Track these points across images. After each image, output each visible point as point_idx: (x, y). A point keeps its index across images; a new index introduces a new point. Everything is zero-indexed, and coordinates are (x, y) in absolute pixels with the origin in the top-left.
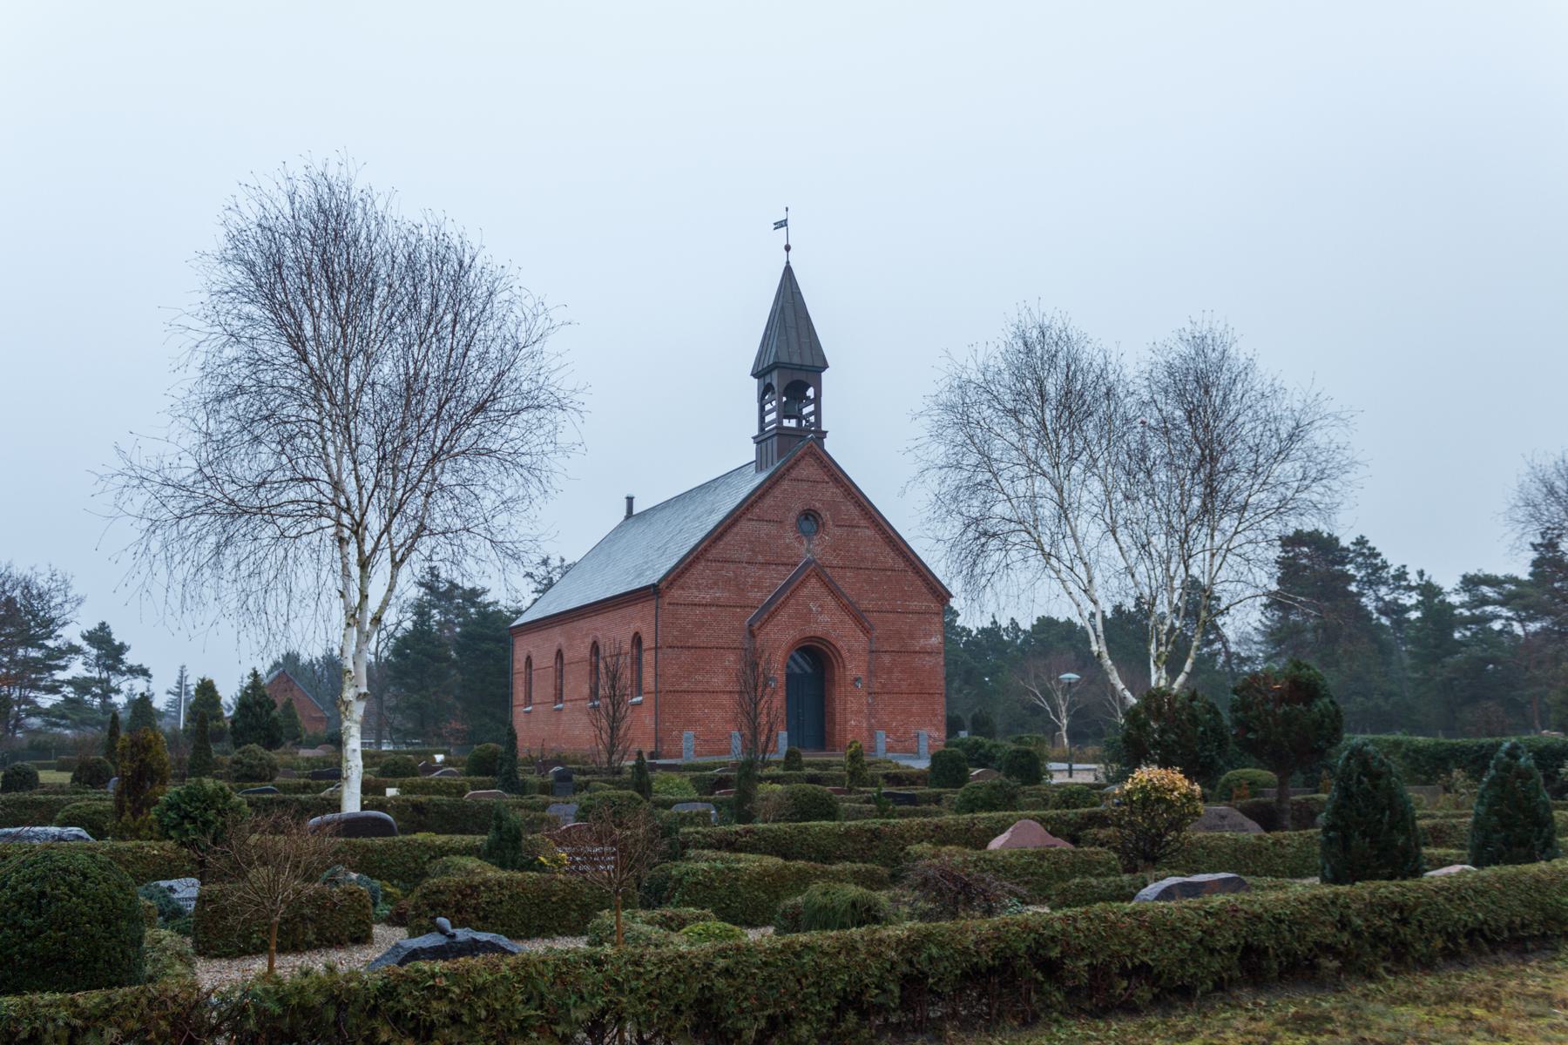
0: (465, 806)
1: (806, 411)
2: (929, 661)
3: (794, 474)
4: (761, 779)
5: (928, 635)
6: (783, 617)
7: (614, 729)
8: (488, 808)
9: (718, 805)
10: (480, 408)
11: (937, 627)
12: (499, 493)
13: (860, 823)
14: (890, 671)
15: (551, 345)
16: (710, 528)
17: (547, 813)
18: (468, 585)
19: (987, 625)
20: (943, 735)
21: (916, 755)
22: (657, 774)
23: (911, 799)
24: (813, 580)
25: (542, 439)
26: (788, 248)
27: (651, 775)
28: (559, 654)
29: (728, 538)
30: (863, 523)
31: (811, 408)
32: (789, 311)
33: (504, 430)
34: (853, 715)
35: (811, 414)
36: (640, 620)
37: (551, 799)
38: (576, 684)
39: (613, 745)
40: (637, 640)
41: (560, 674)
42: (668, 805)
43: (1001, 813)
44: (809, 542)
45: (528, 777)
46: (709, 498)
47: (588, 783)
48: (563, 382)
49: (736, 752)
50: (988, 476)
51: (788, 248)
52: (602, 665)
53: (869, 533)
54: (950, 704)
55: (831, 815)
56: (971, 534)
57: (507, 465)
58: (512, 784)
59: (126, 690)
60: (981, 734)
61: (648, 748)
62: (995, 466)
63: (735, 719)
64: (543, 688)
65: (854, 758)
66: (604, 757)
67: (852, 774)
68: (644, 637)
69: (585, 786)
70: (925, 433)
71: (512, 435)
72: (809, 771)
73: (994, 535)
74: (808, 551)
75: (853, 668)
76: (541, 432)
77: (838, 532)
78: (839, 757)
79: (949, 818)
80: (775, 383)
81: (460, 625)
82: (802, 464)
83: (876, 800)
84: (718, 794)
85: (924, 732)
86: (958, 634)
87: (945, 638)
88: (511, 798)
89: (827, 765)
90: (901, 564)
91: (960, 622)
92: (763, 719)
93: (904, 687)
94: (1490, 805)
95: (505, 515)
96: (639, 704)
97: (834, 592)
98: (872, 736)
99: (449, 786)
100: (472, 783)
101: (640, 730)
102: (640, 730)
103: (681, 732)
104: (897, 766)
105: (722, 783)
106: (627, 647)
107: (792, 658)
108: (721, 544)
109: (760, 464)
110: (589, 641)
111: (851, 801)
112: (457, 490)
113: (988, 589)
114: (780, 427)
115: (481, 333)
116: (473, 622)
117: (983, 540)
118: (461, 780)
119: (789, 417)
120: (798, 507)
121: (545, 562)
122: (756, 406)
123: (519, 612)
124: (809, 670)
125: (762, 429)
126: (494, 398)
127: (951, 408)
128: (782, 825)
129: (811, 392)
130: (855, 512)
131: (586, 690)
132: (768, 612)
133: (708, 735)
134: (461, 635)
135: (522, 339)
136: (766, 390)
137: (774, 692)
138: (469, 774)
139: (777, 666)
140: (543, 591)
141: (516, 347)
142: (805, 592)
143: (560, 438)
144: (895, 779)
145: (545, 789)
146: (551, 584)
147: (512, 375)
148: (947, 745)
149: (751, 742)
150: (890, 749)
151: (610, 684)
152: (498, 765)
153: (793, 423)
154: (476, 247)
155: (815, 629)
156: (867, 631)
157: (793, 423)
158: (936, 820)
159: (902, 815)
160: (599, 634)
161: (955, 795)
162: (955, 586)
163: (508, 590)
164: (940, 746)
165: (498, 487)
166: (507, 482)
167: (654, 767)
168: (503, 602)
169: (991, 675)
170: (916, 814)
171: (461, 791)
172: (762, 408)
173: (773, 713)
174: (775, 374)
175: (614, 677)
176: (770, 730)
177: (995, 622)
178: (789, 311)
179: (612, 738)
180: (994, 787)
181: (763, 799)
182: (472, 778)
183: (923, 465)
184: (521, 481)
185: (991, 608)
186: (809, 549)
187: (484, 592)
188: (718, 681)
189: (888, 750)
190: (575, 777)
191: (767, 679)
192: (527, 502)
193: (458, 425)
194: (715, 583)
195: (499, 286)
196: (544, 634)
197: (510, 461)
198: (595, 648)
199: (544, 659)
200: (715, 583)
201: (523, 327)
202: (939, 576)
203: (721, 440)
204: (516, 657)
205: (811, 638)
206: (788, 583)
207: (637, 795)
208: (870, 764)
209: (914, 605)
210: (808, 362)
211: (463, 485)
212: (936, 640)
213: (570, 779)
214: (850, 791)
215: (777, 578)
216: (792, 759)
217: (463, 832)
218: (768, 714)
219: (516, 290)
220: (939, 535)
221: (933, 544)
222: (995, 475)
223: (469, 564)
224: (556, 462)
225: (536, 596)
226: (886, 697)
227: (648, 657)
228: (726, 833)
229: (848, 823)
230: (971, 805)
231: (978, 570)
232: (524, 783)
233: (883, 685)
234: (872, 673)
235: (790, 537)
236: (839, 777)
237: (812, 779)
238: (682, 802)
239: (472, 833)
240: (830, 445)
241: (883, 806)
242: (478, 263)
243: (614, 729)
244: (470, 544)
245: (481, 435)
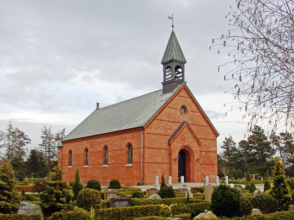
26: (173, 26)
28: (87, 150)
29: (162, 113)
51: (173, 26)
53: (199, 114)
59: (28, 148)
90: (206, 124)
94: (20, 190)
108: (161, 115)
120: (181, 105)
122: (163, 73)
139: (176, 155)
142: (184, 131)
155: (186, 143)
172: (165, 74)
186: (185, 118)
189: (209, 182)
196: (78, 143)
215: (175, 127)
233: (203, 162)
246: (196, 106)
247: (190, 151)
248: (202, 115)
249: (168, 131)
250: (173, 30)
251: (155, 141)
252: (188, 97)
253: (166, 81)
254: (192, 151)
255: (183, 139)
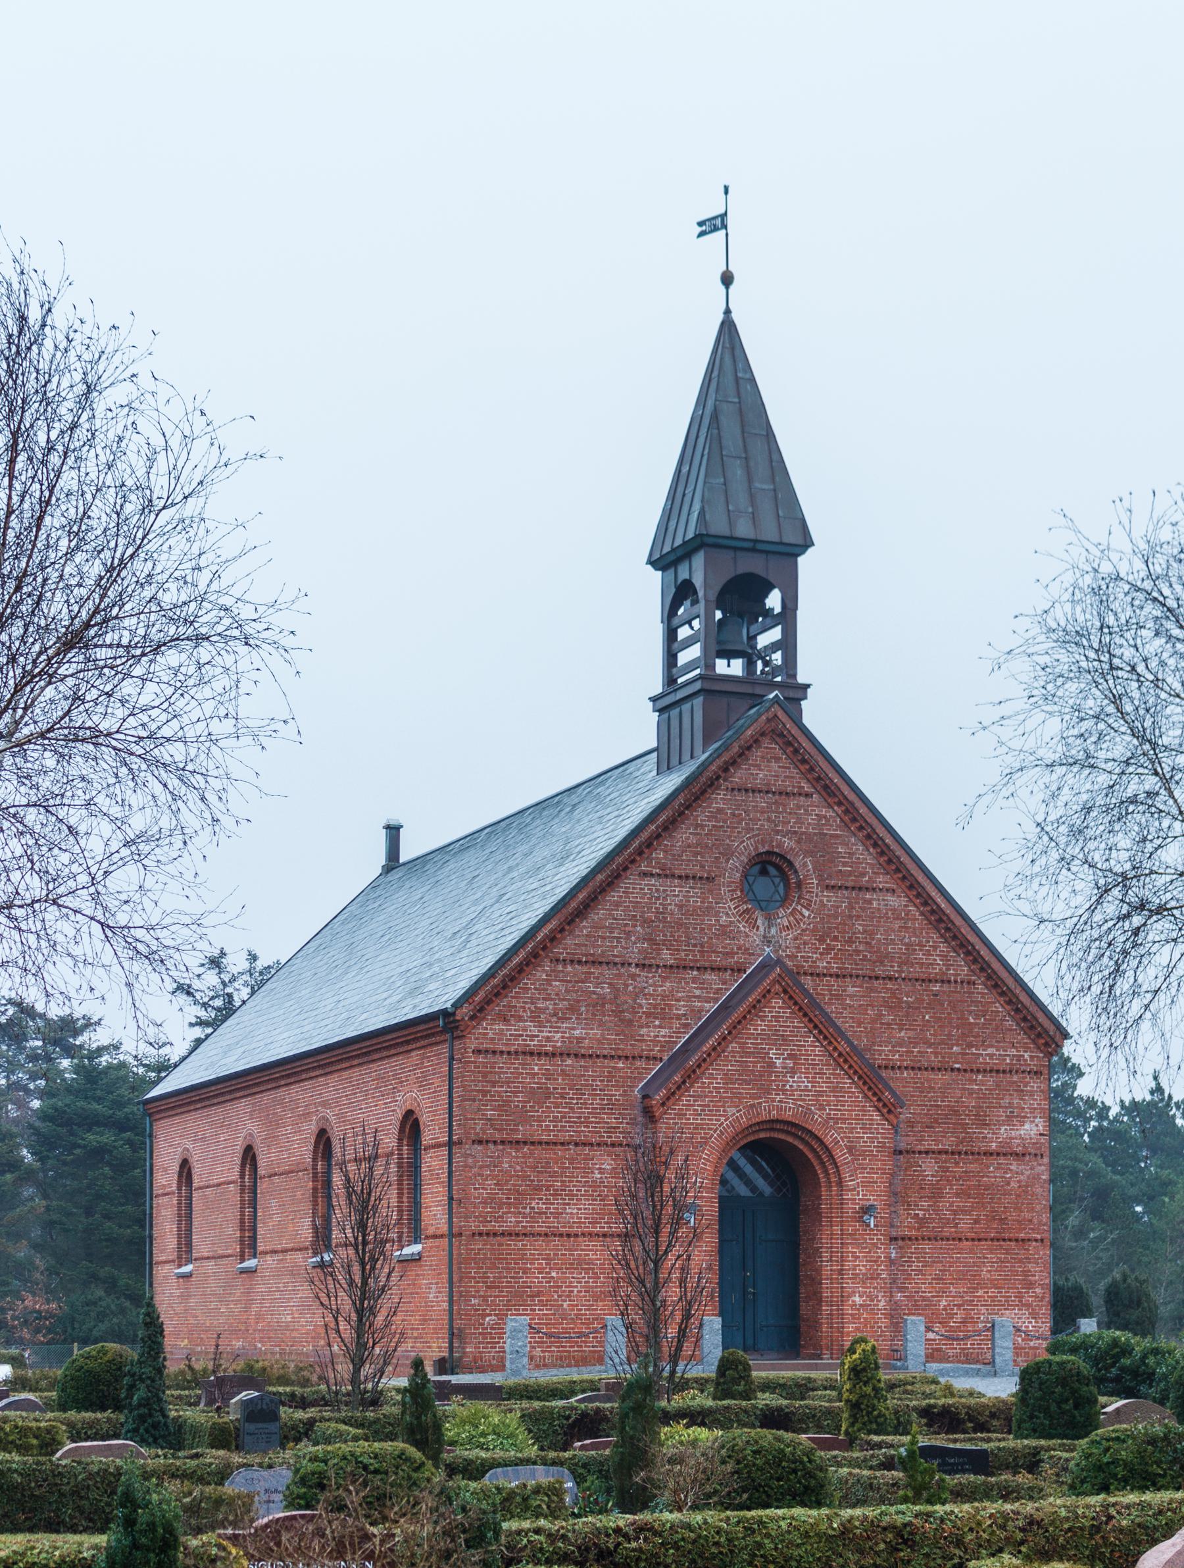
0: (57, 1473)
1: (764, 640)
2: (1019, 1172)
3: (738, 777)
4: (667, 1418)
5: (1016, 1117)
6: (713, 1079)
7: (364, 1312)
8: (109, 1479)
9: (580, 1471)
10: (74, 640)
11: (1037, 1101)
12: (119, 823)
13: (871, 1512)
14: (936, 1193)
15: (219, 505)
16: (561, 892)
17: (229, 1489)
18: (55, 1011)
19: (1142, 1094)
20: (1045, 1326)
21: (990, 1367)
22: (453, 1407)
23: (979, 1462)
24: (777, 1003)
25: (209, 707)
26: (727, 279)
27: (441, 1407)
28: (249, 1156)
29: (599, 914)
30: (882, 880)
31: (774, 634)
32: (730, 421)
33: (128, 688)
34: (855, 1281)
35: (774, 647)
36: (418, 1086)
37: (236, 1459)
38: (287, 1217)
39: (361, 1345)
40: (411, 1126)
41: (251, 1198)
42: (475, 1470)
43: (1165, 1496)
44: (770, 919)
45: (189, 1413)
46: (560, 828)
47: (311, 1423)
48: (249, 584)
49: (615, 1362)
50: (1151, 783)
51: (727, 279)
52: (337, 1179)
54: (1061, 1261)
55: (810, 1490)
56: (1111, 908)
57: (135, 763)
58: (156, 1429)
60: (1124, 1327)
61: (436, 1349)
62: (1167, 762)
63: (614, 1293)
64: (216, 1228)
65: (861, 1373)
66: (344, 1368)
67: (855, 1406)
68: (424, 1119)
69: (304, 1431)
70: (1019, 691)
71: (144, 700)
72: (765, 1399)
73: (1161, 910)
74: (767, 940)
75: (860, 1184)
76: (207, 692)
77: (829, 899)
78: (827, 1371)
79: (1056, 1503)
80: (698, 581)
81: (42, 1094)
82: (756, 754)
83: (905, 1464)
84: (579, 1449)
85: (1006, 1320)
86: (1080, 1115)
87: (1052, 1122)
88: (152, 1458)
89: (802, 1389)
90: (961, 969)
91: (1084, 1088)
92: (672, 1293)
93: (965, 1224)
95: (132, 870)
96: (416, 1259)
97: (821, 1026)
98: (897, 1326)
99: (24, 1432)
100: (71, 1425)
101: (418, 1311)
102: (418, 1311)
103: (502, 1316)
104: (949, 1391)
105: (587, 1425)
106: (389, 1141)
107: (732, 1164)
108: (585, 927)
109: (666, 756)
110: (311, 1127)
111: (852, 1463)
112: (32, 816)
113: (1145, 1025)
114: (709, 676)
115: (68, 481)
116: (69, 1089)
117: (1137, 920)
118: (47, 1419)
119: (728, 655)
120: (746, 847)
121: (215, 962)
123: (164, 1068)
124: (767, 1190)
125: (670, 680)
126: (102, 618)
127: (1073, 637)
128: (712, 1516)
129: (774, 600)
130: (866, 857)
131: (305, 1232)
132: (683, 1067)
133: (555, 1324)
134: (43, 1115)
135: (160, 485)
136: (680, 595)
137: (696, 1235)
138: (63, 1408)
139: (700, 1179)
140: (215, 1024)
141: (148, 506)
142: (759, 1027)
143: (246, 707)
144: (944, 1418)
145: (223, 1438)
146: (228, 1010)
147: (140, 567)
148: (1054, 1349)
149: (647, 1336)
150: (934, 1355)
151: (356, 1230)
152: (122, 1386)
153: (736, 668)
154: (53, 283)
156: (888, 1109)
157: (736, 668)
158: (1030, 1507)
159: (959, 1495)
160: (330, 1114)
161: (1070, 1454)
162: (1077, 1018)
163: (137, 1021)
164: (1040, 1349)
165: (116, 811)
166: (135, 800)
167: (446, 1391)
168: (129, 1046)
169: (1149, 1199)
170: (986, 1493)
171: (49, 1444)
172: (671, 634)
173: (692, 1282)
174: (699, 560)
175: (364, 1206)
176: (687, 1316)
177: (1159, 1089)
178: (730, 421)
179: (360, 1331)
180: (1152, 1441)
181: (672, 1461)
182: (72, 1415)
183: (1014, 762)
184: (163, 797)
185: (1150, 1062)
187: (89, 1024)
188: (577, 1212)
189: (931, 1357)
190: (285, 1412)
191: (680, 1208)
192: (178, 841)
193: (28, 677)
194: (573, 1009)
195: (107, 370)
196: (217, 1113)
197: (140, 754)
198: (323, 1143)
199: (217, 1167)
200: (573, 1009)
201: (161, 465)
202: (1043, 996)
203: (579, 697)
204: (159, 1161)
205: (772, 1124)
206: (725, 1008)
207: (412, 1451)
208: (892, 1386)
209: (989, 1054)
210: (769, 532)
211: (41, 805)
212: (1032, 1129)
213: (275, 1417)
214: (849, 1444)
215: (700, 997)
216: (731, 1379)
217: (54, 1526)
218: (682, 1281)
219: (145, 381)
220: (1044, 910)
221: (1028, 921)
222: (1166, 782)
223: (60, 973)
224: (239, 757)
225: (198, 1032)
226: (927, 1247)
227: (433, 1163)
228: (598, 1532)
229: (848, 1513)
230: (1101, 1476)
231: (1124, 985)
232: (180, 1425)
233: (922, 1222)
234: (897, 1197)
235: (728, 910)
236: (829, 1412)
237: (774, 1419)
238: (506, 1464)
239: (74, 1530)
240: (816, 716)
241: (922, 1475)
242: (59, 318)
243: (364, 1312)
244: (63, 929)
245: (77, 698)
246: (875, 845)
247: (814, 1150)
248: (926, 904)
249: (644, 1031)
250: (728, 312)
251: (542, 1095)
252: (807, 788)
253: (680, 681)
254: (831, 1156)
255: (762, 1079)
